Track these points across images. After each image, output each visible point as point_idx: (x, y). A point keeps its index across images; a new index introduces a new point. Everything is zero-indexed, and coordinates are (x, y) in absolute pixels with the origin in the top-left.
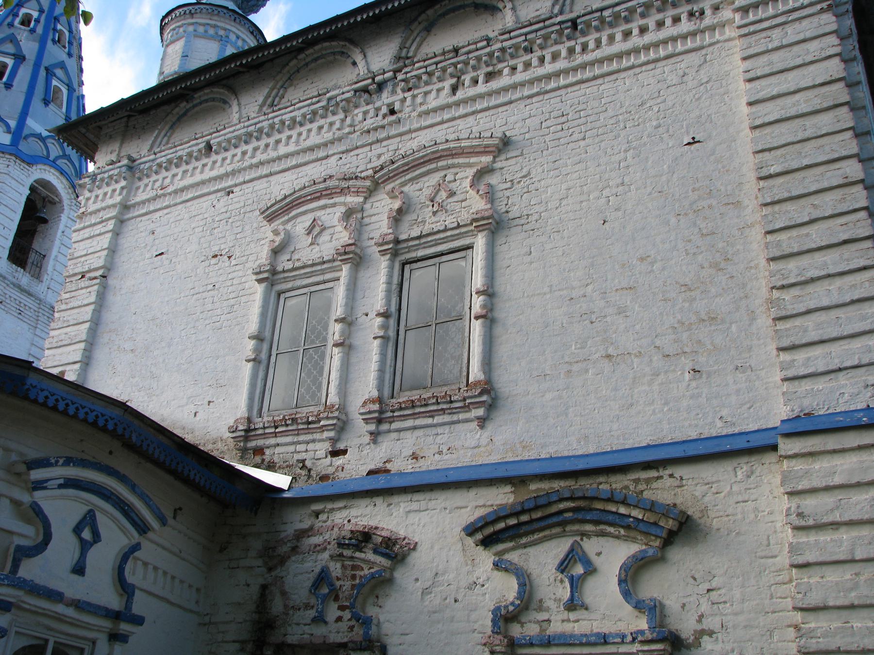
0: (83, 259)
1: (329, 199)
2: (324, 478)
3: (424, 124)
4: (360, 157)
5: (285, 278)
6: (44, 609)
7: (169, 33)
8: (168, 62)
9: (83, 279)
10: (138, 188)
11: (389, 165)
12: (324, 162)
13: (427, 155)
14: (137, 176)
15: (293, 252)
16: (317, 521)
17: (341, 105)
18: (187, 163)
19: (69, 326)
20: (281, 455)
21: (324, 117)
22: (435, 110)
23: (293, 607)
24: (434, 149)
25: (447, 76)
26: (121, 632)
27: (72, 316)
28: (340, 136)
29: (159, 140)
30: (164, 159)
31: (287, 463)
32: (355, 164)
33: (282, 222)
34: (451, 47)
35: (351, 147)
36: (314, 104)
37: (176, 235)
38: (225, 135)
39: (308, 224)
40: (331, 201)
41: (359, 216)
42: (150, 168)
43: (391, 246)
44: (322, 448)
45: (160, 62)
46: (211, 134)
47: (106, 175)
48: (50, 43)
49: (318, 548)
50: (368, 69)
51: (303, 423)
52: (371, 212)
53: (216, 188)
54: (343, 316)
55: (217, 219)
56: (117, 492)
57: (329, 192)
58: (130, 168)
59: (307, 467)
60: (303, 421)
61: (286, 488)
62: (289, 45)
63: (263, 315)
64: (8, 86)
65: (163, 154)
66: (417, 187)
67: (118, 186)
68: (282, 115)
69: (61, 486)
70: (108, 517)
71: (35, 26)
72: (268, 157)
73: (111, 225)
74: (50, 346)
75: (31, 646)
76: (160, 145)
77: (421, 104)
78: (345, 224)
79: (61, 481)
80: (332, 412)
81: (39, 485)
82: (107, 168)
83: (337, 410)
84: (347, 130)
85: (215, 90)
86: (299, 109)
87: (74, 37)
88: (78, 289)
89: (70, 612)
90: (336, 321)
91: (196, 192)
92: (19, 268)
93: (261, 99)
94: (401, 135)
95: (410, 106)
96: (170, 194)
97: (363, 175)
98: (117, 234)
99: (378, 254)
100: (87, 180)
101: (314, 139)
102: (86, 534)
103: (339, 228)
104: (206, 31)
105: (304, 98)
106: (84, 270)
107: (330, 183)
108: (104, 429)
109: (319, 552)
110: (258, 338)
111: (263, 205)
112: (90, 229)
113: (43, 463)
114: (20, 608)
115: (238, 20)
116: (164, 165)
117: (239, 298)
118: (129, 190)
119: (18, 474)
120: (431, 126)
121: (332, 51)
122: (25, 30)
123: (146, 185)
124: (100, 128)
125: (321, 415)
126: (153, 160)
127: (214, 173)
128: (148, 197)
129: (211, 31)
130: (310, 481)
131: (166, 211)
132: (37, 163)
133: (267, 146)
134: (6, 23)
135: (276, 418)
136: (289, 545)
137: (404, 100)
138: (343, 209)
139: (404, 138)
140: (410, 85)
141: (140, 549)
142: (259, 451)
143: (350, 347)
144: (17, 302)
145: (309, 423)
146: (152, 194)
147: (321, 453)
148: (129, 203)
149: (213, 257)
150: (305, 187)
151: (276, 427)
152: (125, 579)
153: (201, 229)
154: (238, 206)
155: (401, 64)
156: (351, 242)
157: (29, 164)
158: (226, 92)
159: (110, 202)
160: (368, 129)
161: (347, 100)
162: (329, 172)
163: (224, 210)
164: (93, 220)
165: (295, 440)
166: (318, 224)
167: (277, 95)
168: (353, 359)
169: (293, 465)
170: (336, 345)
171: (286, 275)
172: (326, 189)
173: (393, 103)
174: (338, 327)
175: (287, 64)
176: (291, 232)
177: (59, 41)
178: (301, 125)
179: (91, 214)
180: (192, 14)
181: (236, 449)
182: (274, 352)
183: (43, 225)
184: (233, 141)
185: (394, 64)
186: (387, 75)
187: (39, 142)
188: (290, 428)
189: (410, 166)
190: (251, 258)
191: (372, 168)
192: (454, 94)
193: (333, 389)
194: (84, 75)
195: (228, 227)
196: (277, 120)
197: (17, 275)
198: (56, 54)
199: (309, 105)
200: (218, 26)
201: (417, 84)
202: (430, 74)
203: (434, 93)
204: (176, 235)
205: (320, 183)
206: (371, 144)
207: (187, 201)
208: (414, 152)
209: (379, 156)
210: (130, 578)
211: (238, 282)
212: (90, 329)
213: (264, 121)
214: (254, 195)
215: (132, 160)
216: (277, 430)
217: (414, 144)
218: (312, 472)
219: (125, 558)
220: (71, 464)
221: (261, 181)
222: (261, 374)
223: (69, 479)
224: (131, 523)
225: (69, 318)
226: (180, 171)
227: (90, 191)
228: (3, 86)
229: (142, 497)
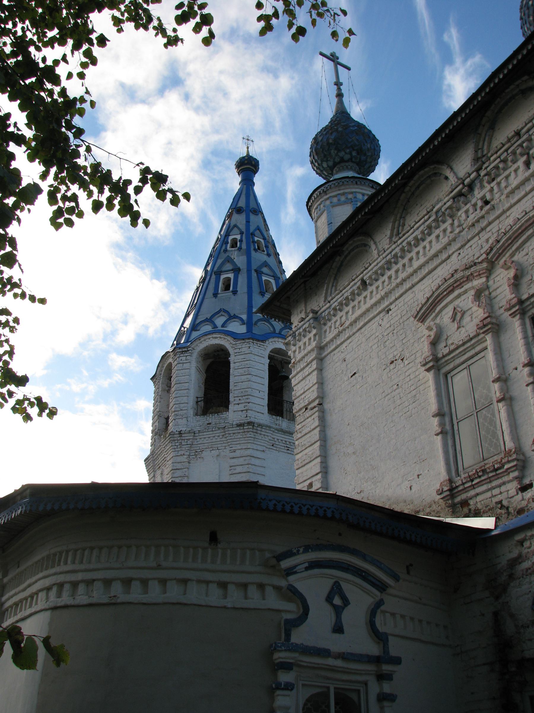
0: (303, 396)
1: (461, 288)
2: (520, 511)
3: (513, 201)
4: (473, 247)
5: (446, 361)
6: (318, 664)
7: (314, 212)
8: (320, 232)
9: (307, 411)
10: (325, 331)
11: (496, 245)
12: (448, 261)
13: (523, 224)
14: (322, 322)
15: (446, 339)
16: (523, 548)
17: (447, 213)
18: (353, 301)
19: (306, 448)
20: (482, 502)
21: (437, 227)
22: (518, 187)
23: (522, 626)
24: (526, 218)
25: (519, 156)
26: (384, 672)
27: (306, 440)
28: (453, 237)
29: (329, 291)
30: (336, 304)
31: (489, 507)
32: (471, 254)
33: (432, 319)
34: (513, 133)
35: (464, 242)
36: (426, 221)
37: (360, 357)
38: (372, 269)
39: (451, 314)
40: (463, 290)
41: (487, 293)
42: (329, 313)
43: (517, 308)
44: (512, 487)
45: (315, 235)
46: (362, 273)
47: (301, 330)
48: (253, 252)
49: (529, 571)
50: (457, 178)
51: (491, 472)
52: (495, 286)
53: (378, 311)
54: (498, 376)
55: (385, 334)
56: (353, 563)
57: (458, 283)
58: (316, 319)
59: (504, 506)
60: (491, 469)
61: (492, 527)
62: (393, 185)
63: (439, 395)
64: (235, 292)
65: (334, 300)
66: (523, 253)
67: (311, 335)
68: (407, 238)
69: (307, 569)
70: (351, 584)
71: (241, 245)
72: (407, 274)
73: (314, 365)
74: (298, 467)
75: (312, 696)
76: (331, 294)
77: (506, 187)
78: (477, 303)
79: (306, 565)
80: (510, 456)
81: (290, 572)
82: (300, 324)
83: (514, 453)
84: (457, 230)
85: (355, 239)
86: (418, 228)
87: (268, 242)
88: (305, 420)
89: (339, 663)
90: (493, 382)
91: (365, 319)
92: (278, 417)
93: (388, 233)
94: (498, 217)
95: (498, 192)
96: (348, 327)
97: (480, 260)
98: (320, 370)
99: (510, 317)
100: (290, 338)
101: (436, 247)
102: (337, 601)
103: (475, 308)
104: (339, 200)
105: (419, 218)
106: (306, 404)
107: (457, 276)
108: (333, 518)
109: (531, 574)
110: (440, 414)
111: (414, 312)
112: (302, 373)
113: (288, 554)
114: (300, 666)
115: (358, 183)
116: (338, 308)
117: (418, 389)
118: (320, 335)
119: (273, 567)
120: (519, 200)
121: (428, 175)
122: (235, 250)
123: (331, 327)
124: (288, 298)
125: (503, 461)
126: (329, 307)
127: (374, 300)
128: (333, 335)
129: (343, 198)
130: (510, 517)
131: (348, 341)
132: (268, 339)
133: (404, 265)
134: (222, 251)
135: (470, 474)
136: (505, 574)
137: (492, 190)
138: (472, 292)
139: (501, 219)
140: (493, 176)
141: (384, 604)
142: (465, 503)
143: (511, 399)
144: (284, 442)
145: (496, 470)
146: (336, 332)
147: (512, 492)
148: (322, 344)
149: (391, 363)
150: (440, 286)
151: (472, 481)
152: (378, 630)
153: (376, 346)
154: (397, 318)
155: (480, 163)
156: (486, 315)
157: (262, 341)
158: (364, 238)
159: (309, 348)
160: (472, 223)
161: (450, 208)
162: (454, 268)
163: (388, 325)
164: (302, 365)
165: (490, 487)
166: (458, 311)
167: (399, 225)
168: (516, 408)
169: (493, 508)
170: (499, 401)
171: (446, 358)
172: (456, 281)
173: (484, 196)
174: (497, 386)
175: (399, 199)
176: (441, 324)
177: (259, 248)
178: (423, 240)
179: (299, 361)
180: (326, 192)
181: (447, 507)
182: (455, 422)
183: (286, 381)
184: (379, 272)
185: (474, 165)
186: (473, 176)
187: (266, 323)
188: (483, 478)
189: (512, 239)
190: (418, 355)
191: (484, 253)
192: (529, 168)
193: (507, 438)
194: (283, 265)
195: (395, 337)
196: (404, 244)
197: (278, 423)
198: (259, 257)
199: (423, 223)
200: (346, 193)
201: (497, 173)
202: (505, 161)
203: (513, 175)
204: (360, 357)
205: (449, 279)
206: (478, 234)
207: (361, 328)
208: (512, 227)
209: (487, 241)
210: (381, 628)
211: (414, 376)
212: (321, 445)
213: (396, 248)
214: (406, 306)
215: (315, 312)
216: (473, 483)
217: (510, 221)
218: (510, 509)
219: (373, 613)
220: (310, 550)
221: (407, 294)
222: (450, 442)
223: (312, 562)
224: (371, 585)
225: (305, 443)
226: (350, 308)
227: (294, 345)
228: (231, 293)
229: (373, 562)
